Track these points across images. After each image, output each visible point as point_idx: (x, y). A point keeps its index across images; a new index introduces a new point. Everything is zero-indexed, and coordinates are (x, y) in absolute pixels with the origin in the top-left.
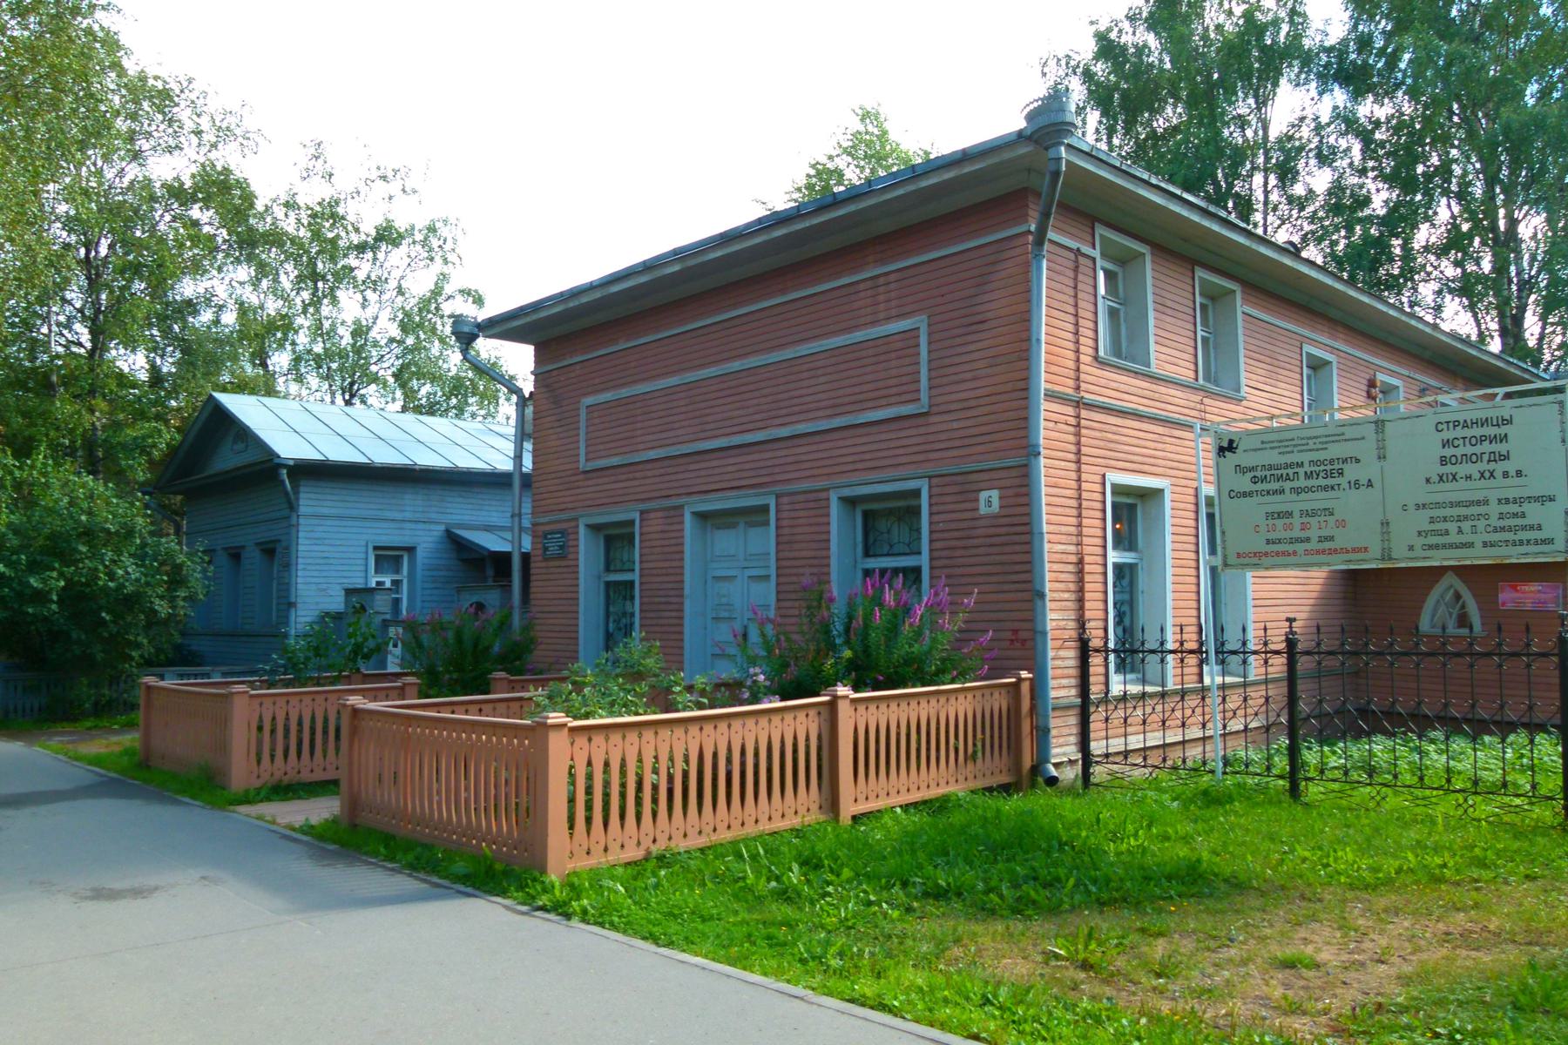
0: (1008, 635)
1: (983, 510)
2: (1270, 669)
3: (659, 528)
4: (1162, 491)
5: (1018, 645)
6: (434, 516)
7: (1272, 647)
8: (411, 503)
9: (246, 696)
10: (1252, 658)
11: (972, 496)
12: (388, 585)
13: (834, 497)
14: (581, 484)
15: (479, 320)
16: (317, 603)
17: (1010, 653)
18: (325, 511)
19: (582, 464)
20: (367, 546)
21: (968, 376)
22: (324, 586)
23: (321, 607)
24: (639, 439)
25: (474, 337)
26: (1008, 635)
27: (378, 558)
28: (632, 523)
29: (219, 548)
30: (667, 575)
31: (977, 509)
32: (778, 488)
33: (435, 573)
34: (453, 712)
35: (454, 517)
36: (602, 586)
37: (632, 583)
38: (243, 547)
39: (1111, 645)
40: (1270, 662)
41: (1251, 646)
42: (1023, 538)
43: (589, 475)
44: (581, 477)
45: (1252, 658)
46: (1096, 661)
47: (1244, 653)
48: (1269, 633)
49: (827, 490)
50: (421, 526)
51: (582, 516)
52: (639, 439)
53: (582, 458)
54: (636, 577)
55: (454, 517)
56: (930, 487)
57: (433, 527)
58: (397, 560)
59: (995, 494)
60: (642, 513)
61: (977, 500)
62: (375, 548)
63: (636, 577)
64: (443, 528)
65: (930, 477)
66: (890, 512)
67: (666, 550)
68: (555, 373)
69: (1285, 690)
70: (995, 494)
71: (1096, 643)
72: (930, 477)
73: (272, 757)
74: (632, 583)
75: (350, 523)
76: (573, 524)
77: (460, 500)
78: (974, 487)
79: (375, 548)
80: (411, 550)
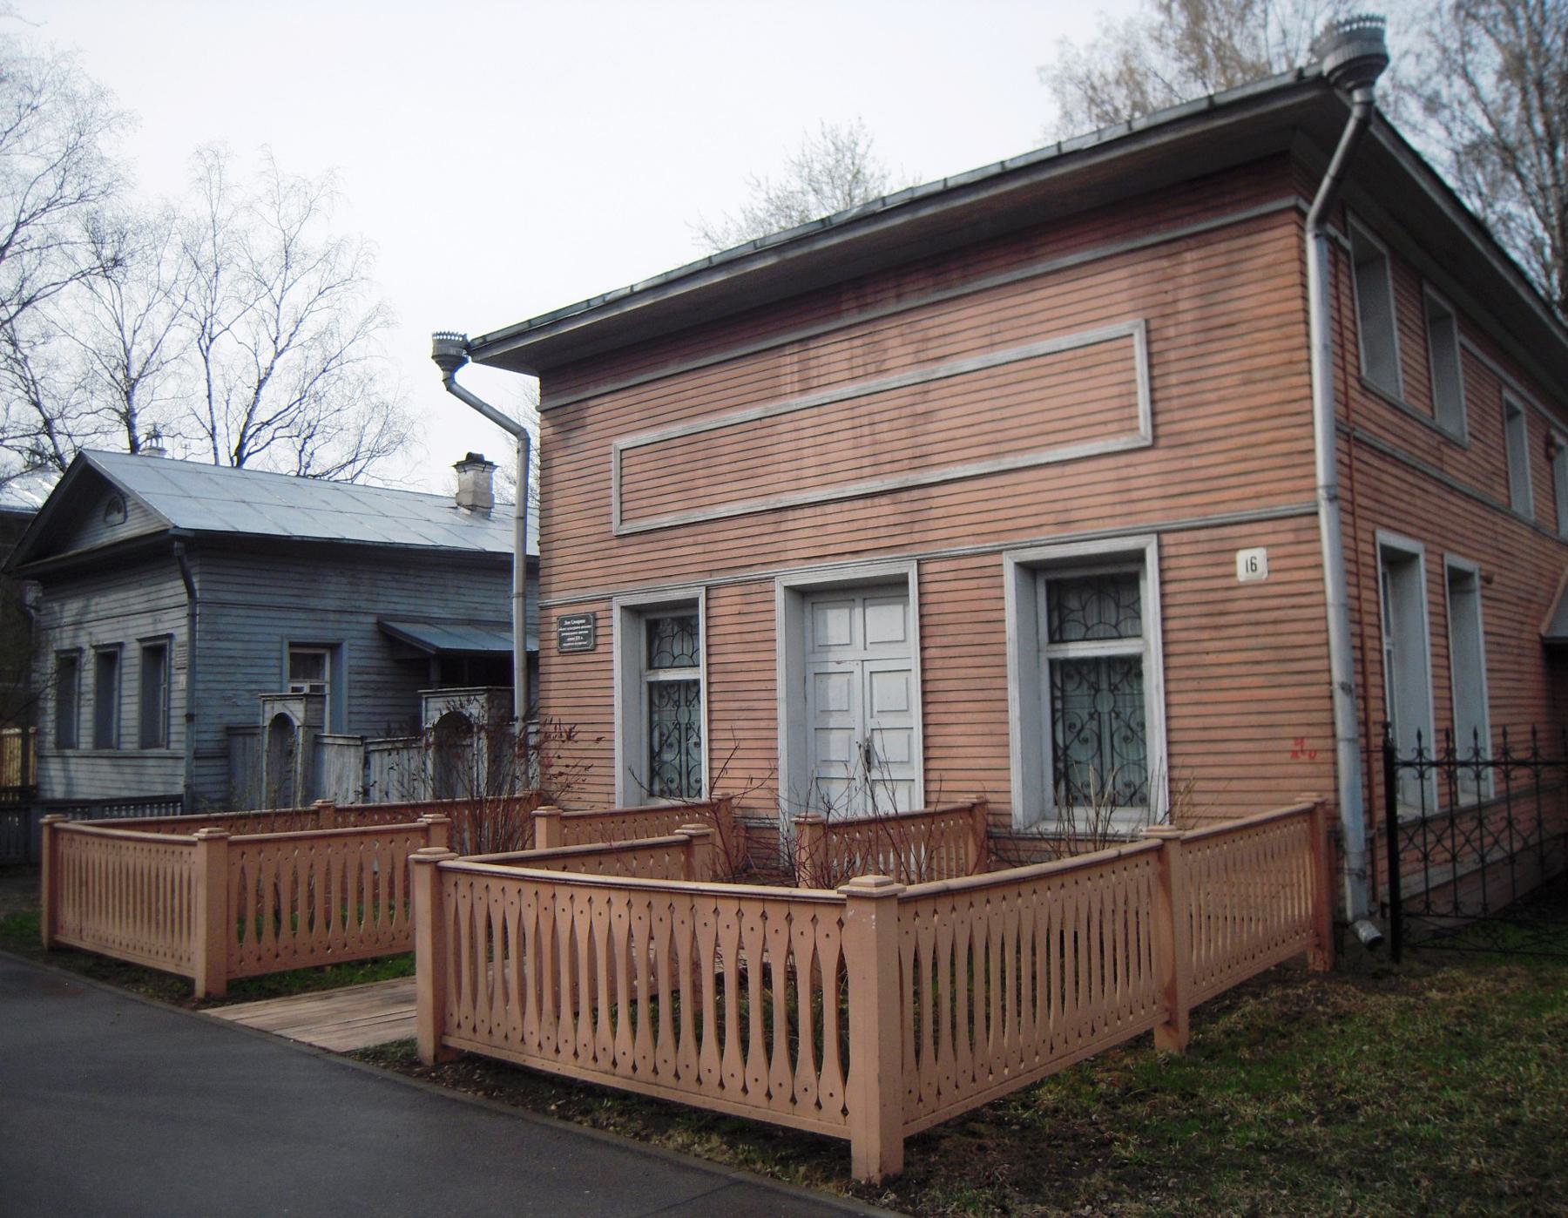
0: (1290, 745)
1: (1242, 574)
2: (1512, 784)
3: (736, 609)
4: (1414, 557)
5: (1304, 758)
6: (364, 604)
7: (1515, 756)
8: (333, 592)
9: (224, 845)
10: (1460, 771)
11: (1226, 557)
12: (306, 690)
13: (1008, 564)
14: (614, 552)
15: (469, 338)
16: (221, 716)
17: (1291, 769)
18: (230, 597)
19: (616, 528)
20: (282, 642)
21: (1212, 396)
22: (230, 694)
23: (226, 720)
24: (701, 492)
25: (462, 362)
26: (1290, 745)
27: (293, 657)
28: (693, 603)
29: (86, 646)
30: (1275, 622)
31: (1234, 575)
32: (919, 551)
33: (365, 677)
34: (564, 869)
35: (398, 607)
36: (645, 688)
37: (696, 682)
38: (121, 645)
39: (1488, 755)
40: (1513, 774)
41: (1459, 756)
42: (995, 649)
43: (628, 541)
44: (615, 543)
45: (1460, 771)
46: (1406, 776)
47: (1421, 764)
48: (1510, 739)
49: (1000, 552)
50: (347, 617)
51: (617, 595)
52: (701, 492)
53: (615, 518)
54: (700, 674)
55: (398, 607)
56: (1160, 546)
57: (361, 618)
58: (317, 661)
59: (1260, 554)
60: (708, 589)
61: (1234, 563)
62: (292, 645)
63: (700, 674)
64: (372, 619)
65: (1159, 533)
66: (1086, 583)
67: (749, 637)
68: (571, 408)
69: (861, 815)
70: (1260, 554)
71: (1405, 753)
72: (1159, 533)
73: (259, 933)
74: (696, 682)
75: (262, 613)
76: (603, 605)
77: (394, 584)
78: (1227, 545)
79: (292, 645)
80: (334, 648)
